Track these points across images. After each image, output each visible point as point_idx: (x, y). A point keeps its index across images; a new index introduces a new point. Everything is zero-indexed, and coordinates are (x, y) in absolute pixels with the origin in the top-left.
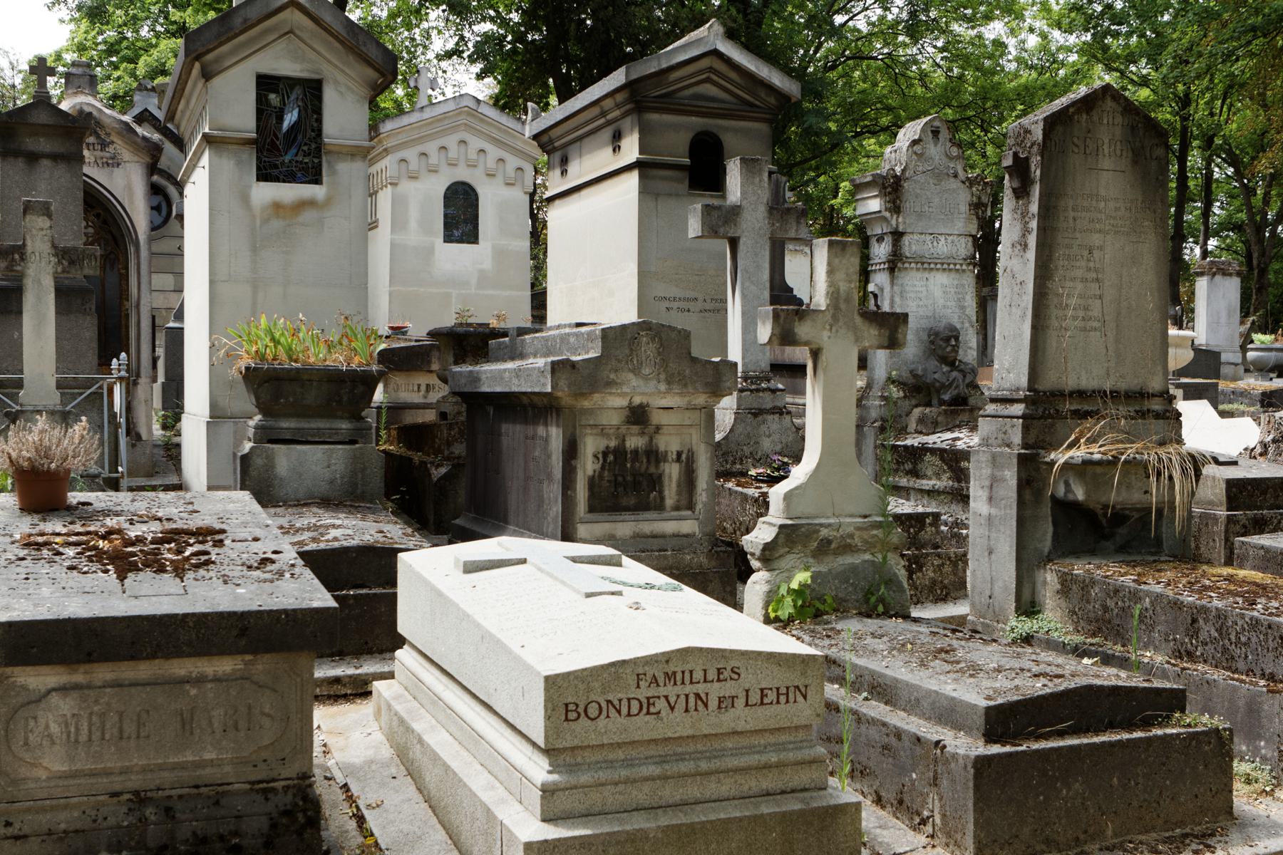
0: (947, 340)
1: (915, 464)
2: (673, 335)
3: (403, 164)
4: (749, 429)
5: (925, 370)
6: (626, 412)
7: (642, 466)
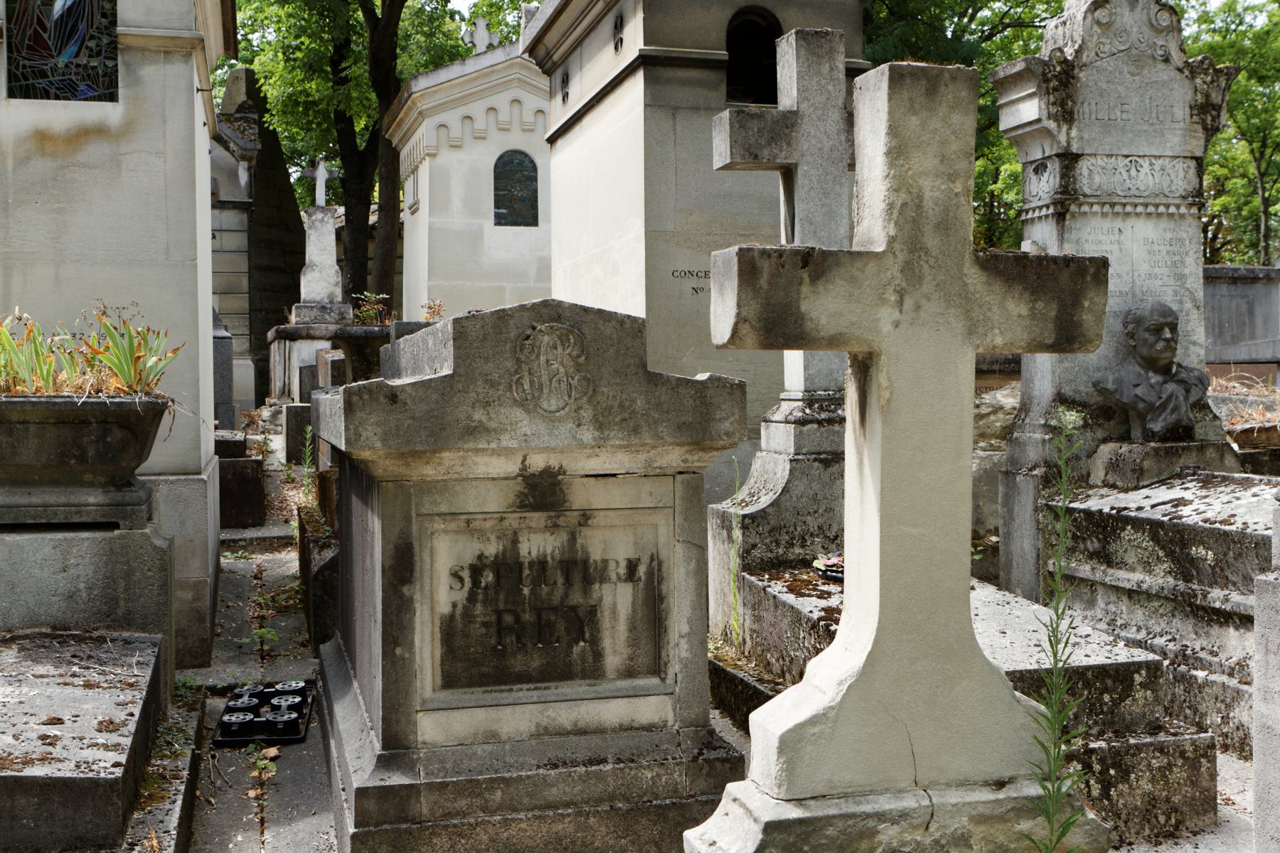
0: (1158, 330)
1: (1105, 542)
2: (609, 329)
3: (443, 130)
4: (816, 486)
5: (1119, 381)
6: (518, 486)
7: (555, 592)
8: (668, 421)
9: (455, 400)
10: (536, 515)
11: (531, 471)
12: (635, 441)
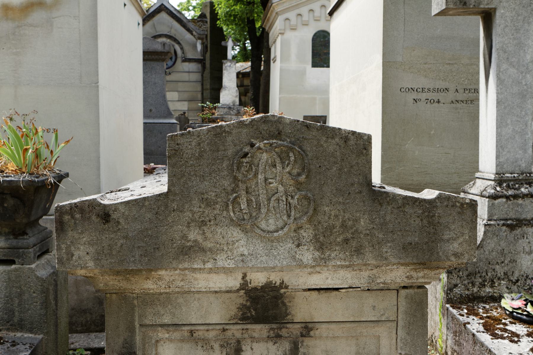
2: (331, 146)
3: (287, 21)
4: (503, 244)
6: (240, 299)
8: (393, 241)
9: (170, 219)
10: (258, 327)
11: (253, 285)
12: (357, 261)
